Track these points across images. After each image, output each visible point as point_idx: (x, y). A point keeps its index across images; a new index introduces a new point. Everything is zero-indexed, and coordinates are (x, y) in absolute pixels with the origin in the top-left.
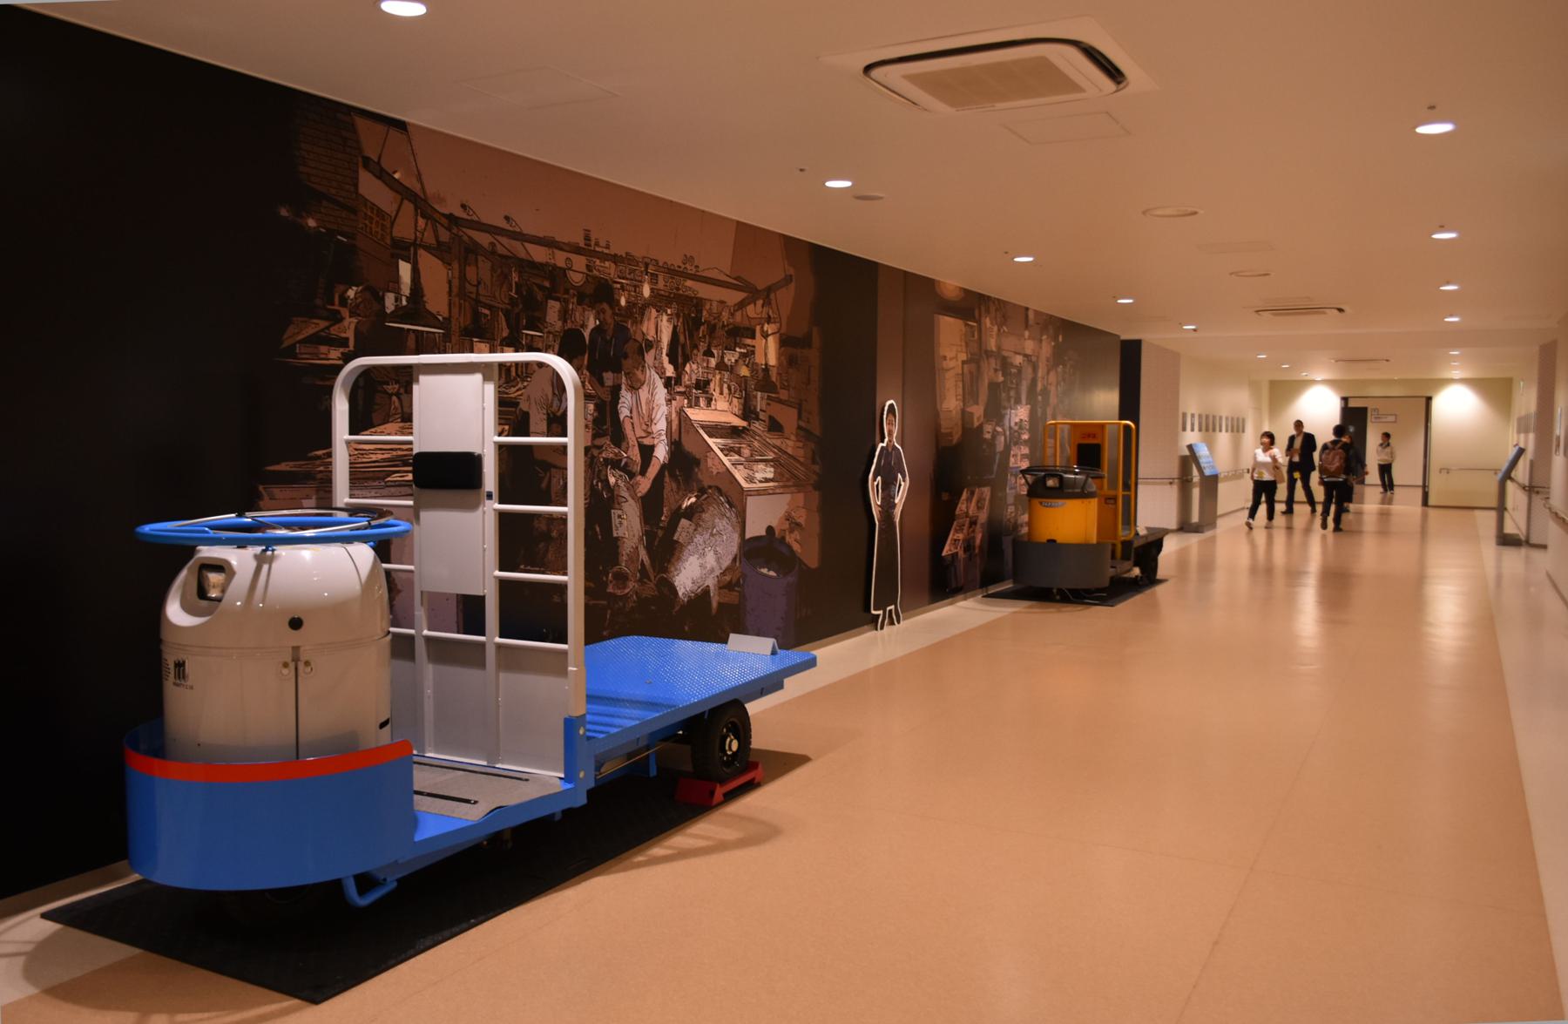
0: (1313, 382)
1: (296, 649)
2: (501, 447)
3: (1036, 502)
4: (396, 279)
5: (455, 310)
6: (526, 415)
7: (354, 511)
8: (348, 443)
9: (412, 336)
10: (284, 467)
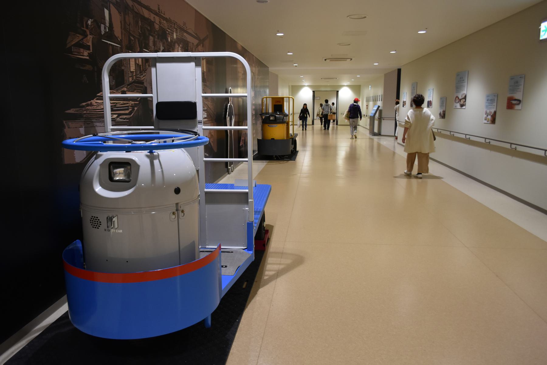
0: (304, 86)
1: (177, 204)
2: (205, 98)
3: (266, 125)
4: (104, 18)
5: (123, 36)
6: (146, 88)
7: (113, 130)
8: (111, 99)
9: (111, 47)
10: (71, 111)
